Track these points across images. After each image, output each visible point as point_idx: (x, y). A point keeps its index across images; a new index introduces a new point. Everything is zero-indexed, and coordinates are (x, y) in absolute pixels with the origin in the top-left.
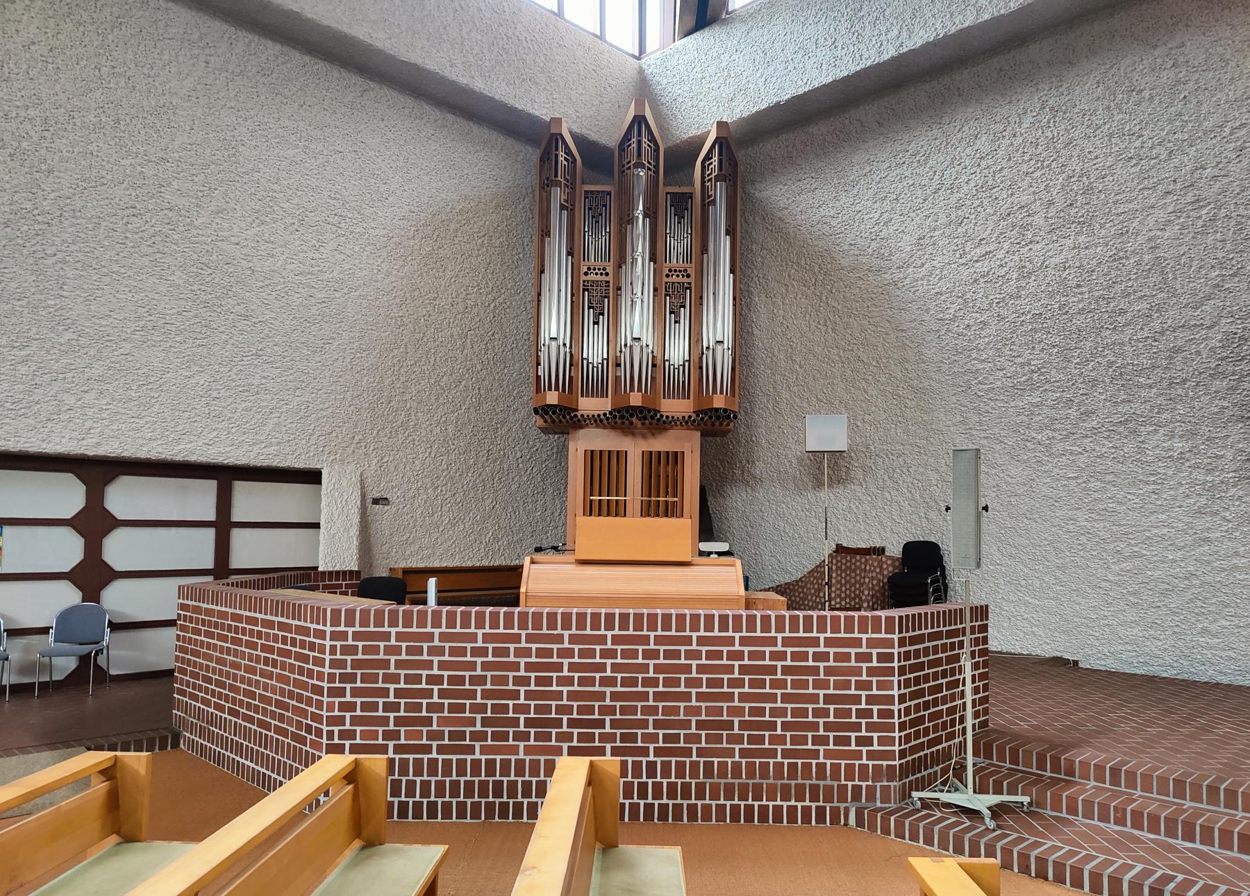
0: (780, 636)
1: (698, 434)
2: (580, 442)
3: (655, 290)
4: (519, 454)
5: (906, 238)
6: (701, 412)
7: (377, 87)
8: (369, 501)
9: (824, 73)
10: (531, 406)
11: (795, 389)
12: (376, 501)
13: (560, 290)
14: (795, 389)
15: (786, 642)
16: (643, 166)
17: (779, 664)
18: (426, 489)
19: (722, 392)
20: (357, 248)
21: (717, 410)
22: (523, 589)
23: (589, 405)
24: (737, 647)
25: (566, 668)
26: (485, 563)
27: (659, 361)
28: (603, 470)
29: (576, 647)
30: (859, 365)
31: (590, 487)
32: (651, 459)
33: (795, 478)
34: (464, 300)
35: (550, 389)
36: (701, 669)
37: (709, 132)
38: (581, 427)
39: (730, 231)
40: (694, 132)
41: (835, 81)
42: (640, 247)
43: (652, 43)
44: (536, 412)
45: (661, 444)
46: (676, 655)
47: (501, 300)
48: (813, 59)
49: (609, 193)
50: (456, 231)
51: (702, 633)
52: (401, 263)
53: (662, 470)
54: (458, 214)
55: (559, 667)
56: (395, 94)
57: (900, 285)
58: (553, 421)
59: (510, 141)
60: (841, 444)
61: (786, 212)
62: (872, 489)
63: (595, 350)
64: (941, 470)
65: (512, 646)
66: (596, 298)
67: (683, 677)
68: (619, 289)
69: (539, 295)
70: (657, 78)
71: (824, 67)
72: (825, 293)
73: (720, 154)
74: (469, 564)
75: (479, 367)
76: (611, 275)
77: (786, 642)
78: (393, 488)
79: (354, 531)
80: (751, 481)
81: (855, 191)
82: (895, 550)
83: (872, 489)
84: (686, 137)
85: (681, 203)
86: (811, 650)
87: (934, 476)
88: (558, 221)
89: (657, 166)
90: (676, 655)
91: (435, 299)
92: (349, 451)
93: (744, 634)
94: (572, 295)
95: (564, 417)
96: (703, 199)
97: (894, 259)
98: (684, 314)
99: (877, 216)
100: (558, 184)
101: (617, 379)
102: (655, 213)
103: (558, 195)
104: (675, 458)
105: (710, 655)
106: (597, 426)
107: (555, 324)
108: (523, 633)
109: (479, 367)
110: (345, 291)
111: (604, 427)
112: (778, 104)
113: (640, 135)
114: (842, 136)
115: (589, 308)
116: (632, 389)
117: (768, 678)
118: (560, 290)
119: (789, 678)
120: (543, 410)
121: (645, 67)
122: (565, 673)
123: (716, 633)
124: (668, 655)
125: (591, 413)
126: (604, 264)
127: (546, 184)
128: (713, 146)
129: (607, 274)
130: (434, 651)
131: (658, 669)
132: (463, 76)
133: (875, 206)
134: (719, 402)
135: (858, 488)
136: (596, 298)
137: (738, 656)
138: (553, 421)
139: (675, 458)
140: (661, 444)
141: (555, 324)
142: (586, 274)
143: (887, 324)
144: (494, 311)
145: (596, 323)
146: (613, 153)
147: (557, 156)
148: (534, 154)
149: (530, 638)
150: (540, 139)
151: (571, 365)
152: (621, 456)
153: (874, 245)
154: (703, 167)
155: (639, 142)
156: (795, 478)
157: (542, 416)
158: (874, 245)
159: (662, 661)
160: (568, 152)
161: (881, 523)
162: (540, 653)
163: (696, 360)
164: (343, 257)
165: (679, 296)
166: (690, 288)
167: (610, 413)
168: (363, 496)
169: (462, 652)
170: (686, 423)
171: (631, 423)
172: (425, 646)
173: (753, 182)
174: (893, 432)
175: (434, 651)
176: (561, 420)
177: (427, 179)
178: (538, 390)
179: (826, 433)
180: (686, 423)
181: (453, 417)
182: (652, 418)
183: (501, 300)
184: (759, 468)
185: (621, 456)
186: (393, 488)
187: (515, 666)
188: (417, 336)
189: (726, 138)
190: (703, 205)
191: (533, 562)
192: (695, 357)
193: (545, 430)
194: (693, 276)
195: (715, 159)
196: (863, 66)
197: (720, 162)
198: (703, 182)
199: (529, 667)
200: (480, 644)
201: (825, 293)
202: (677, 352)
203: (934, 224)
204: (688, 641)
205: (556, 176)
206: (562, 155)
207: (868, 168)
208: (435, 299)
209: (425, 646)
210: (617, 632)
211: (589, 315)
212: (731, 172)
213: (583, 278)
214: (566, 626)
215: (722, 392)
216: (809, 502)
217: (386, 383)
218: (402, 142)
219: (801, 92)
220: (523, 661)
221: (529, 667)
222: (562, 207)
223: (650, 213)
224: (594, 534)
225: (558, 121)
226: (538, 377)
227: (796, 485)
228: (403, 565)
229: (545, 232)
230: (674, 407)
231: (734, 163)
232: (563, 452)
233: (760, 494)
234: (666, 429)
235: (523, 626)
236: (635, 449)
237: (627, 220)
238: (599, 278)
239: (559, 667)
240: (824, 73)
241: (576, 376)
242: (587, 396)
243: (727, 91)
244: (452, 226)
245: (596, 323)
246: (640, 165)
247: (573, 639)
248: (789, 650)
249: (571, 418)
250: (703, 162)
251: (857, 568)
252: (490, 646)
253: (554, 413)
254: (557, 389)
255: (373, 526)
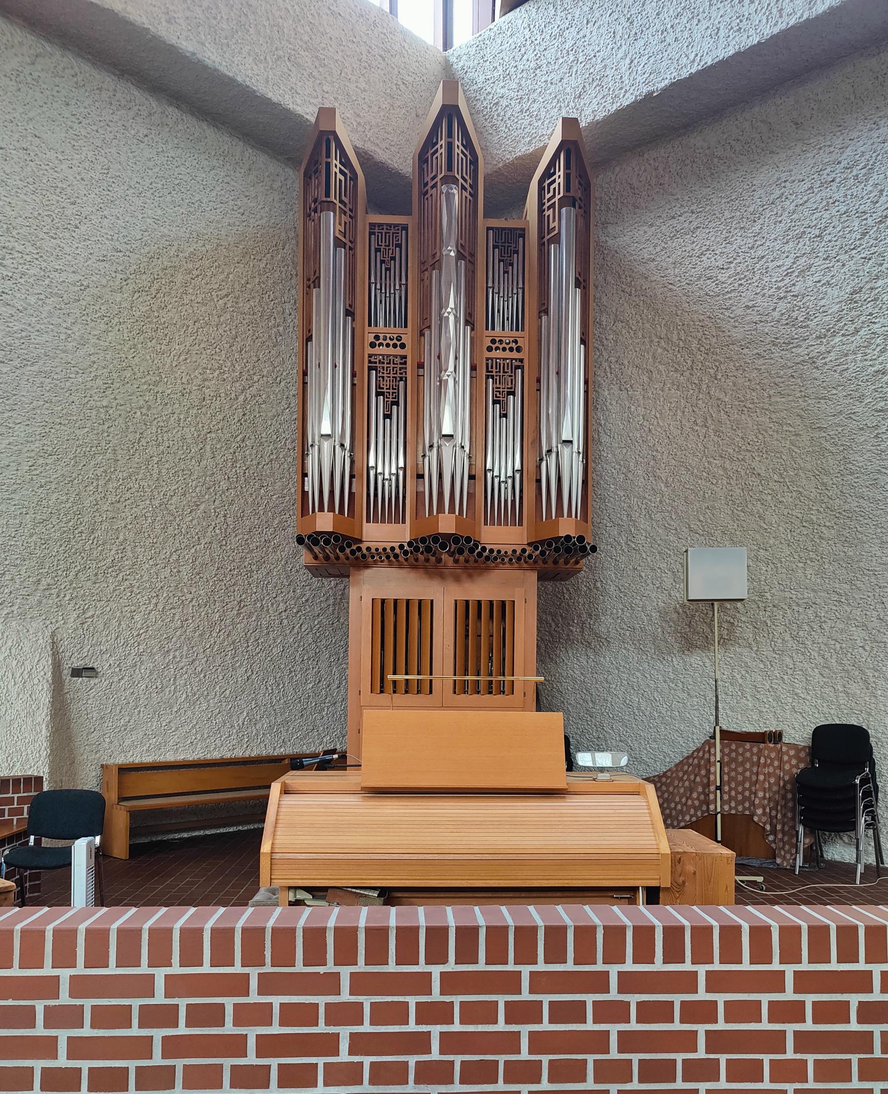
0: (789, 970)
1: (534, 576)
2: (365, 587)
3: (473, 368)
4: (282, 607)
5: (833, 292)
6: (542, 542)
7: (58, 53)
8: (66, 672)
9: (722, 43)
10: (292, 532)
11: (658, 516)
12: (77, 673)
13: (335, 366)
14: (658, 516)
15: (804, 982)
16: (455, 181)
17: (790, 1028)
18: (152, 655)
19: (570, 515)
20: (32, 300)
21: (568, 538)
22: (265, 848)
23: (377, 534)
24: (702, 995)
25: (344, 1045)
26: (239, 753)
27: (479, 473)
28: (401, 629)
29: (367, 1001)
30: (753, 481)
31: (463, 664)
32: (467, 612)
33: (655, 638)
34: (200, 388)
35: (321, 509)
36: (628, 1041)
37: (545, 147)
38: (367, 566)
39: (582, 283)
40: (523, 149)
41: (738, 54)
42: (452, 305)
43: (463, 35)
44: (300, 540)
45: (483, 589)
46: (576, 1012)
47: (253, 390)
48: (705, 24)
49: (405, 228)
50: (185, 284)
51: (629, 966)
52: (103, 327)
53: (484, 627)
54: (190, 258)
55: (329, 1045)
56: (87, 67)
57: (820, 362)
58: (327, 558)
59: (262, 159)
60: (739, 590)
61: (652, 265)
62: (766, 651)
63: (385, 464)
64: (870, 625)
65: (229, 1003)
66: (390, 385)
67: (591, 1058)
68: (421, 366)
69: (305, 374)
70: (470, 75)
71: (722, 34)
72: (706, 380)
73: (567, 166)
74: (216, 755)
75: (224, 485)
76: (408, 346)
77: (804, 982)
78: (102, 653)
79: (43, 716)
80: (594, 642)
81: (757, 228)
82: (799, 733)
83: (766, 651)
84: (510, 157)
85: (508, 242)
86: (854, 999)
87: (859, 635)
88: (331, 261)
89: (475, 186)
90: (576, 1012)
91: (156, 384)
92: (34, 600)
93: (717, 966)
94: (354, 375)
95: (342, 550)
96: (541, 237)
97: (812, 324)
98: (513, 404)
99: (789, 262)
100: (330, 206)
101: (419, 496)
102: (473, 255)
103: (331, 224)
104: (502, 611)
105: (646, 1012)
106: (391, 565)
107: (328, 421)
108: (254, 973)
109: (224, 485)
110: (16, 363)
111: (400, 566)
112: (649, 97)
113: (450, 134)
114: (738, 147)
115: (378, 394)
116: (441, 509)
117: (766, 1058)
118: (335, 366)
119: (810, 1058)
120: (310, 540)
121: (453, 59)
122: (344, 1056)
123: (659, 965)
124: (559, 1012)
125: (380, 546)
126: (399, 330)
127: (313, 209)
128: (556, 156)
129: (403, 346)
130: (60, 1017)
131: (539, 1042)
132: (187, 38)
133: (786, 248)
134: (567, 528)
135: (746, 651)
136: (390, 385)
137: (706, 1012)
138: (327, 558)
139: (502, 611)
140: (483, 589)
141: (328, 421)
142: (373, 345)
143: (798, 421)
144: (243, 407)
145: (388, 416)
146: (410, 185)
147: (328, 165)
148: (294, 178)
149: (268, 985)
150: (308, 153)
151: (352, 476)
152: (424, 608)
153: (782, 306)
154: (541, 189)
155: (450, 146)
156: (655, 638)
157: (311, 550)
158: (782, 306)
159: (546, 1026)
160: (345, 161)
161: (777, 699)
162: (290, 1014)
163: (531, 474)
164: (12, 311)
165: (509, 379)
166: (522, 368)
167: (410, 544)
168: (57, 667)
169: (122, 1017)
170: (519, 559)
171: (439, 560)
172: (40, 1006)
173: (605, 224)
174: (800, 573)
175: (60, 1017)
176: (337, 555)
177: (139, 202)
178: (304, 511)
179: (716, 574)
180: (519, 559)
181: (188, 555)
182: (472, 551)
183: (253, 390)
184: (606, 624)
185: (424, 608)
186: (102, 653)
187: (237, 1046)
188: (131, 436)
189: (575, 143)
190: (541, 245)
191: (286, 791)
192: (530, 466)
193: (315, 571)
194: (526, 349)
195: (560, 177)
196: (782, 26)
197: (567, 177)
198: (541, 211)
199: (266, 1046)
200: (159, 998)
201: (706, 380)
202: (504, 463)
203: (876, 270)
204: (600, 982)
205: (328, 194)
206: (336, 166)
207: (778, 193)
208: (156, 384)
209: (40, 1006)
210: (451, 966)
211: (378, 406)
212: (580, 197)
213: (369, 350)
214: (346, 956)
215: (570, 515)
216: (675, 670)
217: (87, 503)
218: (98, 143)
219: (685, 74)
220: (252, 1033)
221: (266, 1046)
222: (338, 243)
223: (466, 254)
224: (396, 733)
225: (327, 113)
226: (304, 494)
227: (657, 647)
228: (121, 760)
229: (312, 281)
230: (500, 537)
231: (586, 187)
232: (342, 601)
233: (606, 660)
234: (488, 569)
235: (253, 957)
236: (444, 597)
237: (431, 263)
238: (391, 351)
239: (329, 1045)
240: (722, 43)
241: (357, 495)
242: (376, 521)
243: (573, 83)
244: (179, 278)
245: (388, 416)
246: (449, 180)
247: (360, 984)
248: (809, 999)
249: (353, 552)
250: (541, 182)
251: (746, 760)
252: (183, 1003)
253: (327, 542)
254: (331, 509)
255: (73, 707)
